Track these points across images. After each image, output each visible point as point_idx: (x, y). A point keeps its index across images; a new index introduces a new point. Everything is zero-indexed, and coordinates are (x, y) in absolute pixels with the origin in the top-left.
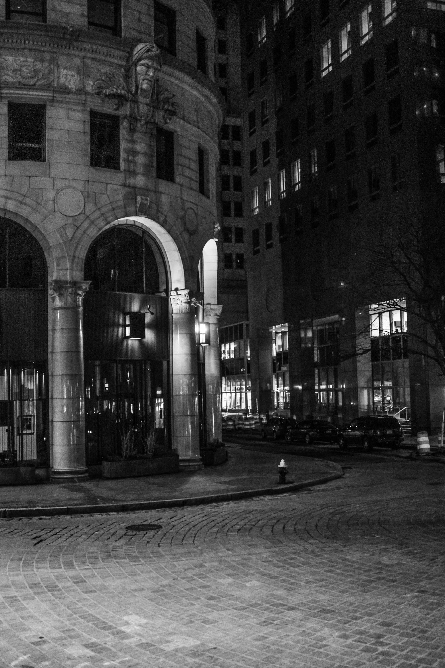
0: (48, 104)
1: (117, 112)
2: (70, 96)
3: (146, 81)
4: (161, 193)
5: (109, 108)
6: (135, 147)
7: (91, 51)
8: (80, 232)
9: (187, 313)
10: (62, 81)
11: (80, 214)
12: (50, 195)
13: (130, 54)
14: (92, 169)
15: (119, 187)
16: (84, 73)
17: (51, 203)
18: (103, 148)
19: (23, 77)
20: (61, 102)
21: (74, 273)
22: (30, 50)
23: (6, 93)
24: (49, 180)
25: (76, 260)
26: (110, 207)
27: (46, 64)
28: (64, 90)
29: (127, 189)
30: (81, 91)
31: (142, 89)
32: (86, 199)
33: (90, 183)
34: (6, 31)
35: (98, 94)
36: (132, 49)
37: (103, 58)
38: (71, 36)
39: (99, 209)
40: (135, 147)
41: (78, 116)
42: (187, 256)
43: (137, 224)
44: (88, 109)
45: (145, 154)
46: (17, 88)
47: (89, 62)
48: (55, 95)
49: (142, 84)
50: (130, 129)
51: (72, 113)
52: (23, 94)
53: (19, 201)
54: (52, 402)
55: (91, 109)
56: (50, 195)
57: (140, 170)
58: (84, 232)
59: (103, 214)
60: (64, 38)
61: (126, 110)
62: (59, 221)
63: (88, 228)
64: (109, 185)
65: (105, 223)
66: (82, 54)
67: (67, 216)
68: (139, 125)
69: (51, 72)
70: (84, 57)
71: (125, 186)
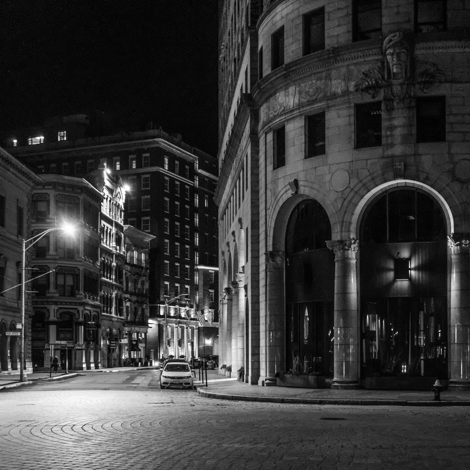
0: (326, 110)
1: (377, 99)
2: (339, 99)
3: (395, 66)
4: (421, 155)
5: (367, 98)
6: (397, 123)
7: (351, 59)
8: (346, 203)
9: (458, 254)
10: (333, 89)
11: (346, 188)
12: (328, 178)
13: (381, 48)
14: (356, 152)
15: (377, 160)
16: (347, 79)
17: (328, 183)
18: (367, 131)
19: (310, 96)
20: (334, 106)
21: (343, 234)
22: (314, 74)
23: (303, 111)
24: (326, 168)
25: (345, 223)
26: (370, 178)
27: (323, 81)
28: (334, 96)
29: (384, 160)
30: (346, 93)
31: (394, 73)
32: (351, 176)
33: (354, 162)
34: (298, 66)
35: (357, 91)
36: (382, 44)
37: (362, 60)
38: (333, 53)
39: (361, 181)
40: (397, 123)
41: (345, 112)
42: (458, 203)
43: (399, 185)
44: (353, 105)
45: (404, 126)
46: (309, 105)
47: (352, 67)
48: (329, 102)
49: (393, 70)
50: (387, 110)
51: (340, 112)
52: (306, 110)
53: (310, 187)
54: (450, 346)
55: (355, 104)
56: (328, 178)
57: (398, 140)
58: (350, 202)
59: (364, 185)
60: (329, 58)
61: (381, 96)
62: (333, 196)
63: (353, 198)
64: (368, 161)
65: (366, 191)
66: (346, 63)
67: (337, 192)
68: (395, 104)
69: (326, 85)
70: (348, 65)
71: (383, 157)
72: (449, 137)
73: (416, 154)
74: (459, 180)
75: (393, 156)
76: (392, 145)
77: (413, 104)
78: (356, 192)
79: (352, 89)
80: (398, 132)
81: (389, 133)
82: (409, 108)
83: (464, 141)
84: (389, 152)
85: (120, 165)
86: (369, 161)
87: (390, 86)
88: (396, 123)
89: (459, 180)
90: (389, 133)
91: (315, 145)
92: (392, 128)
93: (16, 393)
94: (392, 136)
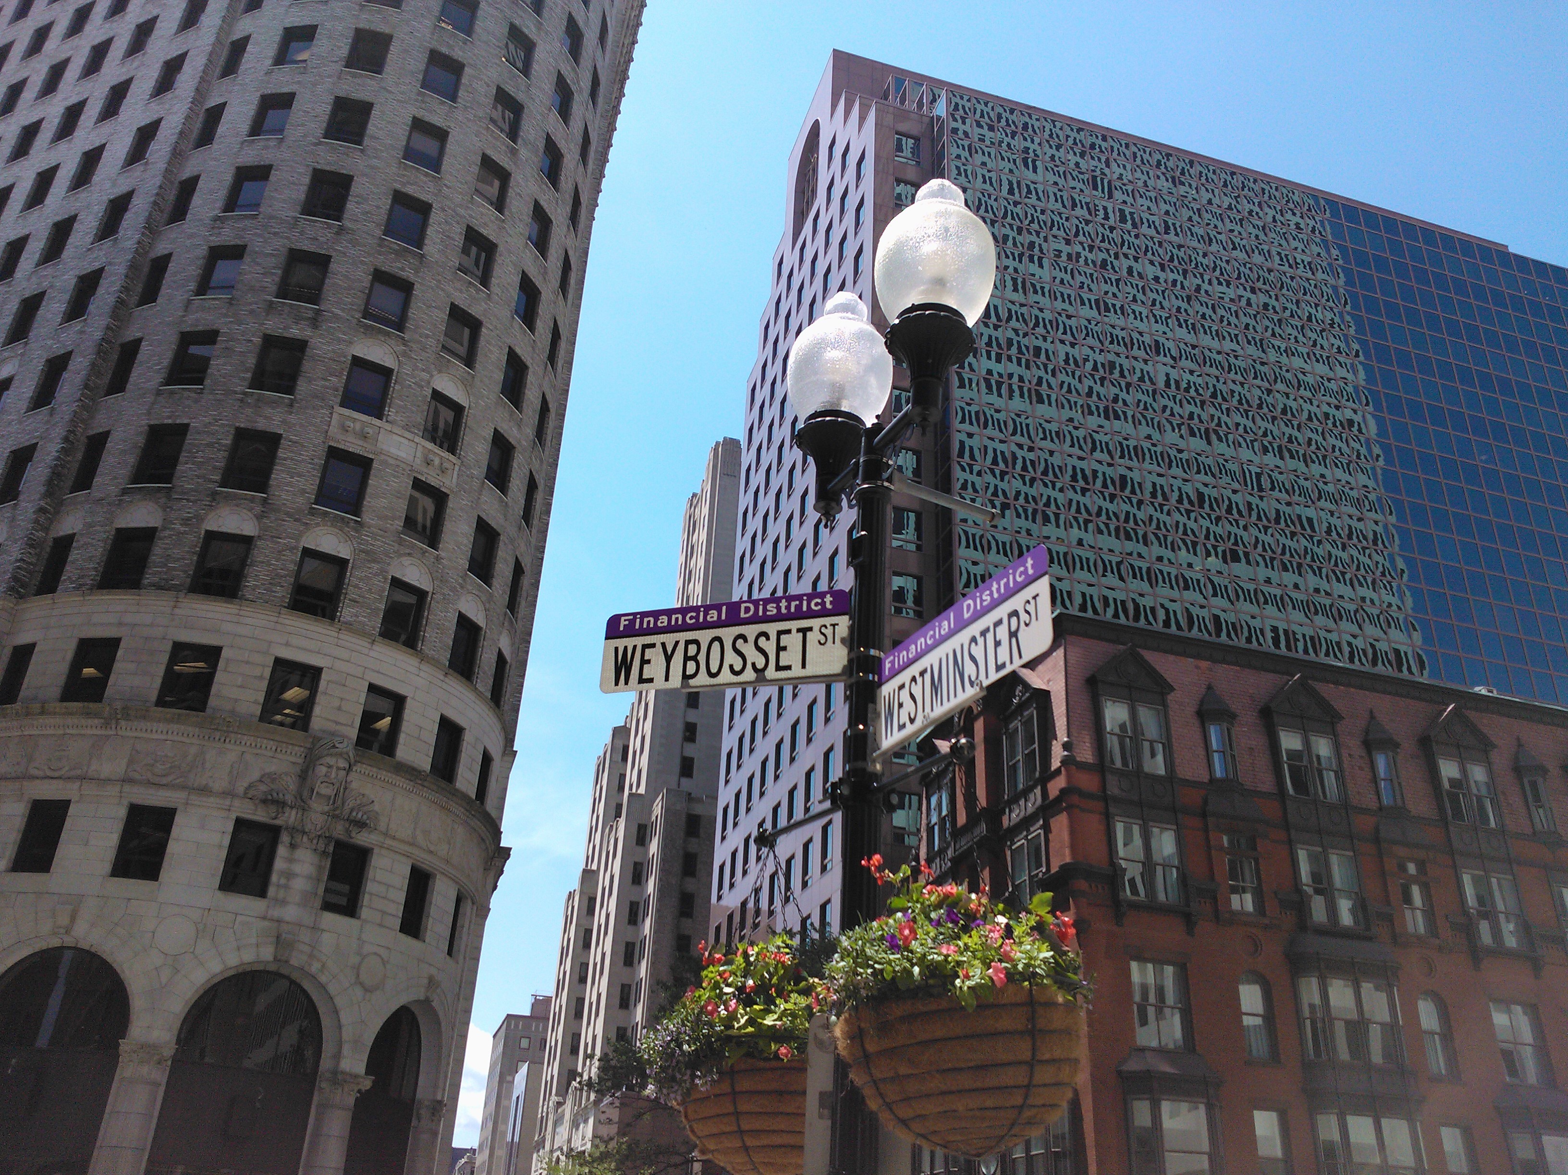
2: (212, 799)
5: (260, 815)
14: (220, 895)
29: (266, 923)
71: (264, 918)
72: (365, 913)
73: (315, 928)
74: (362, 984)
75: (279, 921)
76: (283, 902)
77: (331, 849)
78: (741, 1132)
79: (241, 790)
80: (299, 884)
81: (283, 881)
82: (324, 853)
83: (381, 925)
84: (276, 913)
85: (1238, 1013)
86: (239, 918)
87: (304, 809)
88: (297, 868)
89: (362, 984)
90: (283, 881)
91: (142, 848)
92: (289, 875)
93: (252, 113)
94: (286, 887)
